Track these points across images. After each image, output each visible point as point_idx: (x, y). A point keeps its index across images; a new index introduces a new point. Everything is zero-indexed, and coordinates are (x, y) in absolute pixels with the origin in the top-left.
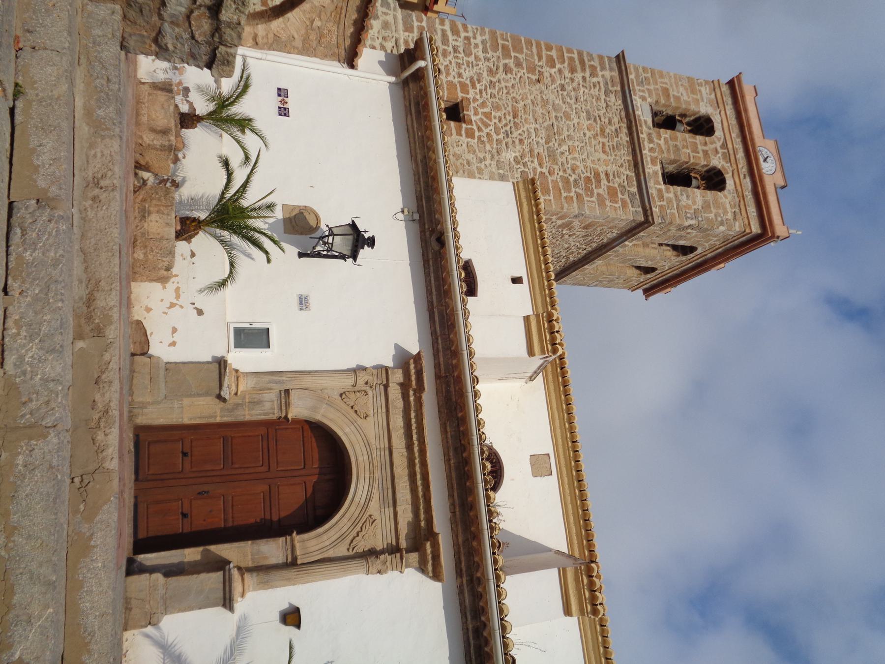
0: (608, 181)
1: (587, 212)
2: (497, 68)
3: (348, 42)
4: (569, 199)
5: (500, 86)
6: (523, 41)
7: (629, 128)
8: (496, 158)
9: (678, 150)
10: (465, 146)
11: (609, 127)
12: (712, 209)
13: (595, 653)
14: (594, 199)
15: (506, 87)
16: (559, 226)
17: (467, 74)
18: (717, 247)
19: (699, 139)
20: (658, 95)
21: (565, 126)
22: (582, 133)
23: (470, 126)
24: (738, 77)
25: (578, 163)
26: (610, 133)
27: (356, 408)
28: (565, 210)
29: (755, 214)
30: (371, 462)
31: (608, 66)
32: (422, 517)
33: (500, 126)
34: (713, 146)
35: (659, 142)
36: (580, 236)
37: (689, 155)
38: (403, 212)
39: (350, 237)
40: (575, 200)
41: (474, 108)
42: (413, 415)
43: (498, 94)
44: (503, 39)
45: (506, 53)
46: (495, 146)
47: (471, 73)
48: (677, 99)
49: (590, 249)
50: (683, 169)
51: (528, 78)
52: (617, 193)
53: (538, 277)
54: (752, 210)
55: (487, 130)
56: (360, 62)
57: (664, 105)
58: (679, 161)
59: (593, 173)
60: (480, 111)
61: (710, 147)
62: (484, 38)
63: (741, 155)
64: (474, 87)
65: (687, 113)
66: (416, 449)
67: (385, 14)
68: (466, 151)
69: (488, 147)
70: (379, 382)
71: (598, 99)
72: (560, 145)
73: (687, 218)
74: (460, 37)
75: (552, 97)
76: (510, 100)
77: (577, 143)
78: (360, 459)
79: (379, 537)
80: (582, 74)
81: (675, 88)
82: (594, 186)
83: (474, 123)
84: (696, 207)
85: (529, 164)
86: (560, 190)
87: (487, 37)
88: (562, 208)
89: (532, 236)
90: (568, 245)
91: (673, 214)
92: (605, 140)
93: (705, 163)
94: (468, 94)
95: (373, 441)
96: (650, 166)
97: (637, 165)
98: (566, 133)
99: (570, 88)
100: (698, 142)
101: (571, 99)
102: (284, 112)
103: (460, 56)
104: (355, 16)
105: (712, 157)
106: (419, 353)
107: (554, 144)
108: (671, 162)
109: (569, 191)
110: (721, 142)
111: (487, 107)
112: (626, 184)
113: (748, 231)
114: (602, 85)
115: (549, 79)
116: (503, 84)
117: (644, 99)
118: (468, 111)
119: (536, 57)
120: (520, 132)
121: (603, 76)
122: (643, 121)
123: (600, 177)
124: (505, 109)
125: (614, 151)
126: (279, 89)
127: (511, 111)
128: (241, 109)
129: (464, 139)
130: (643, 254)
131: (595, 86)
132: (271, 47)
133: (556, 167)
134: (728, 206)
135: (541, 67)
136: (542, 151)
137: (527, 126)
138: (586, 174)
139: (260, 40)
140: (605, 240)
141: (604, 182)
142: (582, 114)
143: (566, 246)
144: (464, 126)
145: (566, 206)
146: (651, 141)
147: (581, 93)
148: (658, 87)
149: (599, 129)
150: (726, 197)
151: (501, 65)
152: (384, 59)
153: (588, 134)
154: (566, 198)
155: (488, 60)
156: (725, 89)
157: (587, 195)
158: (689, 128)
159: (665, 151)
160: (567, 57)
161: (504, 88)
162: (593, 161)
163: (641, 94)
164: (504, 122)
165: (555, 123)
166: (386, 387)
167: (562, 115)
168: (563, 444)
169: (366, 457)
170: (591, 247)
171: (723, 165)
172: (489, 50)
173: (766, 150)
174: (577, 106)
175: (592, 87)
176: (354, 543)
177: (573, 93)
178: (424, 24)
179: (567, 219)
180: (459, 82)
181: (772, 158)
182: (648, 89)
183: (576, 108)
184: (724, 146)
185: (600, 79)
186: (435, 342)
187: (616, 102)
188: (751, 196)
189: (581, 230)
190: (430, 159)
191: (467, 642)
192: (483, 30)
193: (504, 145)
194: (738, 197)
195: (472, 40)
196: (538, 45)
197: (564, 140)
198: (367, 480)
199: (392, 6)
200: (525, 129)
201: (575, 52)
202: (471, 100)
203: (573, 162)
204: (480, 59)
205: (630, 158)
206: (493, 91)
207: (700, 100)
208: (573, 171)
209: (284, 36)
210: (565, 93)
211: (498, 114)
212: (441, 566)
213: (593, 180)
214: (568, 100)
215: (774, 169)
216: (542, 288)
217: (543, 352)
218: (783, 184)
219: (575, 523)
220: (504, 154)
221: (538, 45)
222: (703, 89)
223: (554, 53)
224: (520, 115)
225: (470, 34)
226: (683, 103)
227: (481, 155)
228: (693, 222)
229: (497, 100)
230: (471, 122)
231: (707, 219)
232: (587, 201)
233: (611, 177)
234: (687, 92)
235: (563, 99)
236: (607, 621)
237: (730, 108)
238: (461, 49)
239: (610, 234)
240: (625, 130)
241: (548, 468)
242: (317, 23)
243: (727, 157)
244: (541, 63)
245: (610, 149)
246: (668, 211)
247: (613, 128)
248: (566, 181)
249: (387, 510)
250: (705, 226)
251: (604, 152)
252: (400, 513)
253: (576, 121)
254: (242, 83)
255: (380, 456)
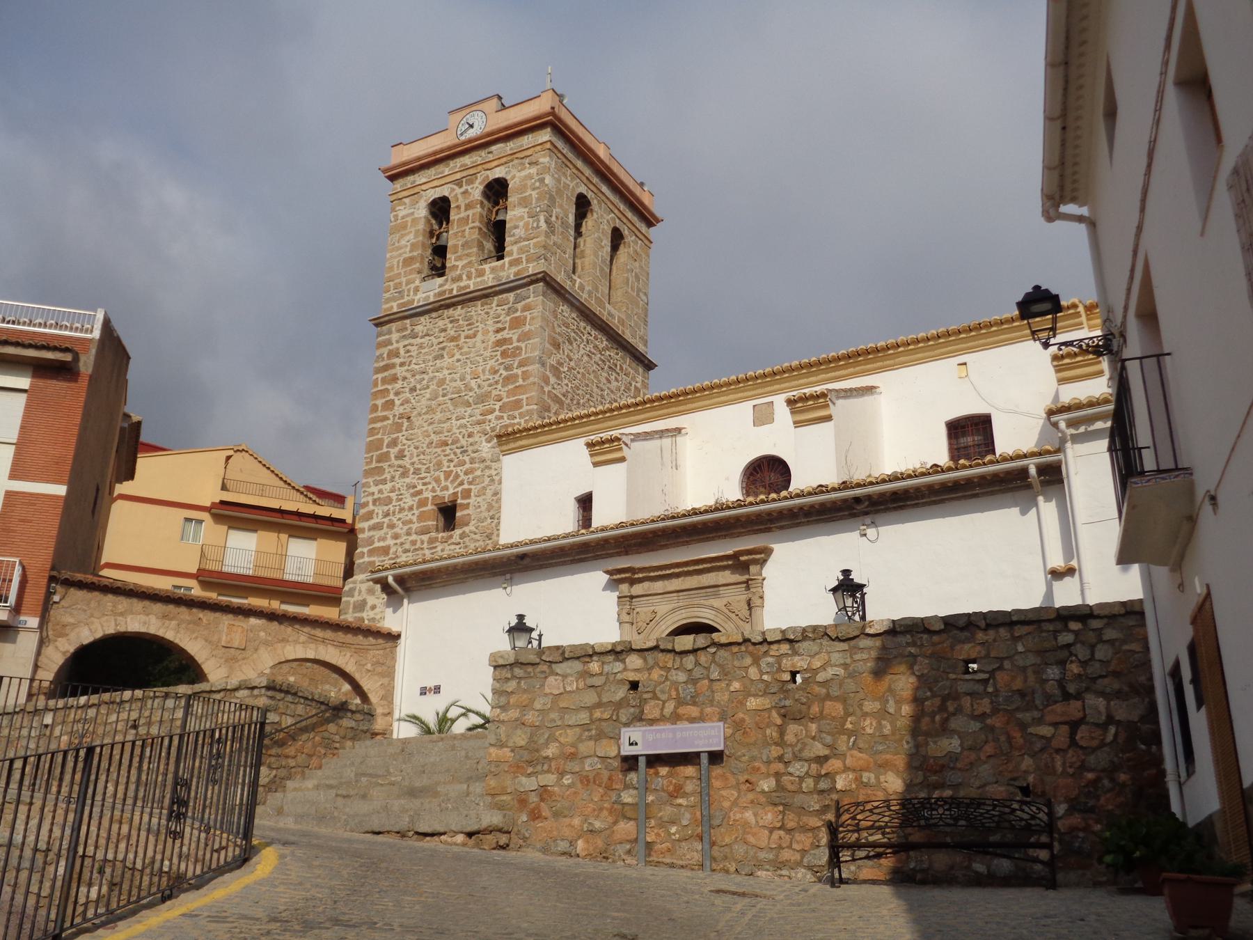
0: (505, 328)
1: (537, 353)
2: (400, 467)
3: (380, 641)
4: (526, 376)
5: (417, 462)
6: (371, 439)
7: (448, 307)
8: (488, 463)
9: (466, 243)
10: (479, 499)
11: (449, 332)
12: (527, 194)
13: (936, 349)
14: (523, 345)
15: (418, 456)
16: (559, 378)
17: (409, 501)
18: (574, 171)
19: (453, 216)
20: (411, 272)
21: (451, 384)
22: (457, 364)
23: (459, 495)
24: (384, 171)
25: (488, 367)
26: (455, 329)
27: (648, 621)
28: (536, 379)
29: (530, 136)
30: (686, 607)
31: (387, 337)
32: (725, 563)
33: (456, 460)
34: (460, 196)
35: (460, 267)
36: (570, 348)
37: (472, 228)
38: (505, 588)
39: (515, 634)
40: (525, 369)
41: (441, 491)
42: (652, 574)
43: (425, 464)
44: (372, 461)
45: (384, 457)
46: (477, 465)
47: (408, 495)
48: (414, 247)
49: (588, 328)
50: (488, 230)
51: (406, 431)
52: (516, 318)
53: (589, 425)
54: (527, 140)
55: (462, 474)
56: (395, 629)
57: (422, 262)
58: (478, 240)
59: (497, 348)
60: (443, 484)
61: (462, 202)
62: (372, 484)
63: (467, 160)
64: (420, 492)
65: (428, 230)
66: (677, 570)
67: (360, 592)
68: (484, 497)
69: (478, 473)
70: (628, 603)
71: (421, 346)
72: (471, 390)
73: (538, 227)
74: (374, 510)
75: (424, 402)
76: (430, 450)
77: (468, 370)
78: (684, 616)
79: (738, 598)
80: (398, 368)
81: (402, 251)
82: (510, 347)
83: (456, 490)
84: (526, 216)
85: (492, 425)
86: (516, 387)
87: (370, 480)
88: (535, 383)
89: (549, 434)
90: (585, 356)
91: (535, 245)
92: (463, 335)
93: (478, 206)
94: (428, 498)
95: (673, 606)
96: (485, 278)
97: (485, 295)
98: (459, 383)
99: (412, 380)
100: (456, 217)
101: (424, 379)
102: (437, 689)
103: (392, 509)
104: (360, 637)
105: (471, 198)
106: (607, 572)
107: (470, 396)
108: (481, 246)
109: (516, 376)
110: (455, 187)
111: (439, 476)
112: (506, 307)
113: (548, 145)
114: (406, 342)
115: (405, 406)
116: (415, 459)
117: (417, 290)
118: (444, 497)
119: (385, 423)
120: (460, 437)
121: (397, 342)
122: (440, 289)
123: (501, 340)
124: (439, 455)
125: (473, 324)
126: (421, 694)
127: (441, 449)
128: (432, 722)
129: (472, 501)
130: (592, 257)
131: (408, 351)
132: (391, 702)
133: (494, 393)
134: (523, 173)
135: (395, 416)
136: (478, 410)
137: (455, 430)
138: (499, 357)
139: (386, 711)
140: (574, 315)
141: (505, 334)
142: (438, 365)
143: (585, 358)
144: (459, 501)
145: (532, 379)
146: (459, 278)
147: (417, 367)
148: (402, 272)
149: (452, 344)
150: (514, 177)
151: (397, 463)
152: (391, 609)
153: (457, 356)
154: (524, 380)
155: (393, 477)
156: (399, 185)
157: (520, 354)
158: (444, 223)
159: (469, 259)
160: (382, 386)
161: (419, 458)
162: (485, 349)
163: (412, 293)
164: (452, 456)
165: (450, 396)
166: (632, 597)
167: (440, 389)
168: (743, 392)
169: (683, 611)
170: (585, 328)
171: (480, 184)
172: (383, 477)
173: (460, 125)
174: (430, 371)
175: (409, 354)
176: (742, 618)
177: (418, 377)
178: (365, 550)
179: (548, 373)
180: (417, 508)
181: (468, 116)
182: (407, 285)
183: (433, 372)
184: (459, 183)
185: (401, 345)
186: (596, 558)
187: (423, 325)
188: (511, 143)
189: (561, 352)
190: (462, 568)
191: (818, 521)
192: (364, 485)
193: (475, 455)
194: (512, 160)
195: (375, 497)
196: (373, 421)
197: (466, 385)
198: (699, 609)
199: (351, 586)
200: (458, 431)
201: (375, 377)
202: (434, 494)
203: (487, 373)
204: (393, 486)
205: (479, 303)
206: (423, 470)
207: (413, 217)
208: (496, 372)
209: (382, 692)
210: (418, 387)
211: (446, 464)
212: (754, 548)
213: (504, 347)
214: (425, 382)
215: (480, 113)
216: (597, 422)
217: (621, 449)
218: (495, 100)
219: (816, 376)
220: (484, 455)
221: (373, 421)
222: (401, 214)
223: (380, 402)
224: (444, 438)
225: (370, 499)
226: (417, 239)
227: (487, 480)
228: (542, 219)
229: (431, 465)
230: (455, 494)
231: (538, 199)
232: (525, 354)
233: (500, 325)
234: (405, 235)
235: (425, 389)
236: (903, 340)
237: (420, 178)
238: (386, 508)
239: (564, 314)
240: (451, 311)
241: (766, 405)
242: (369, 666)
243: (471, 179)
244: (391, 417)
245: (471, 329)
246: (532, 251)
247: (450, 326)
248: (507, 380)
249: (721, 592)
250: (546, 202)
251: (475, 336)
252: (724, 582)
253: (446, 372)
254: (414, 721)
255: (683, 600)
